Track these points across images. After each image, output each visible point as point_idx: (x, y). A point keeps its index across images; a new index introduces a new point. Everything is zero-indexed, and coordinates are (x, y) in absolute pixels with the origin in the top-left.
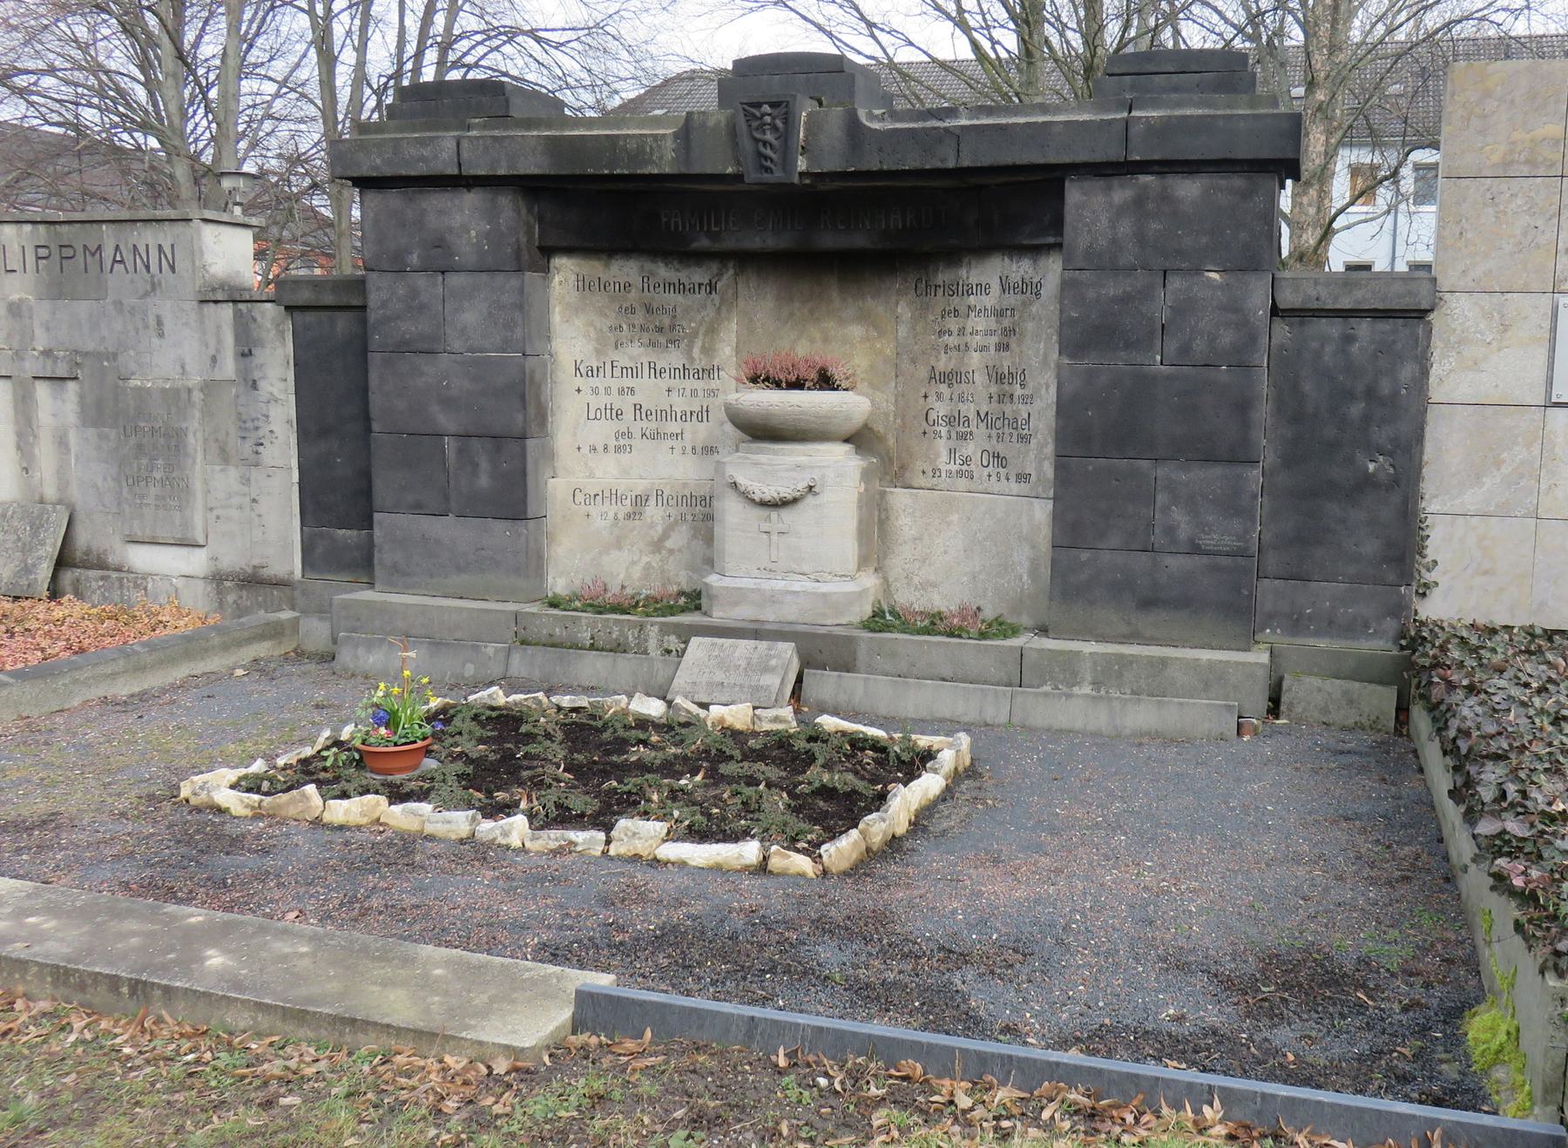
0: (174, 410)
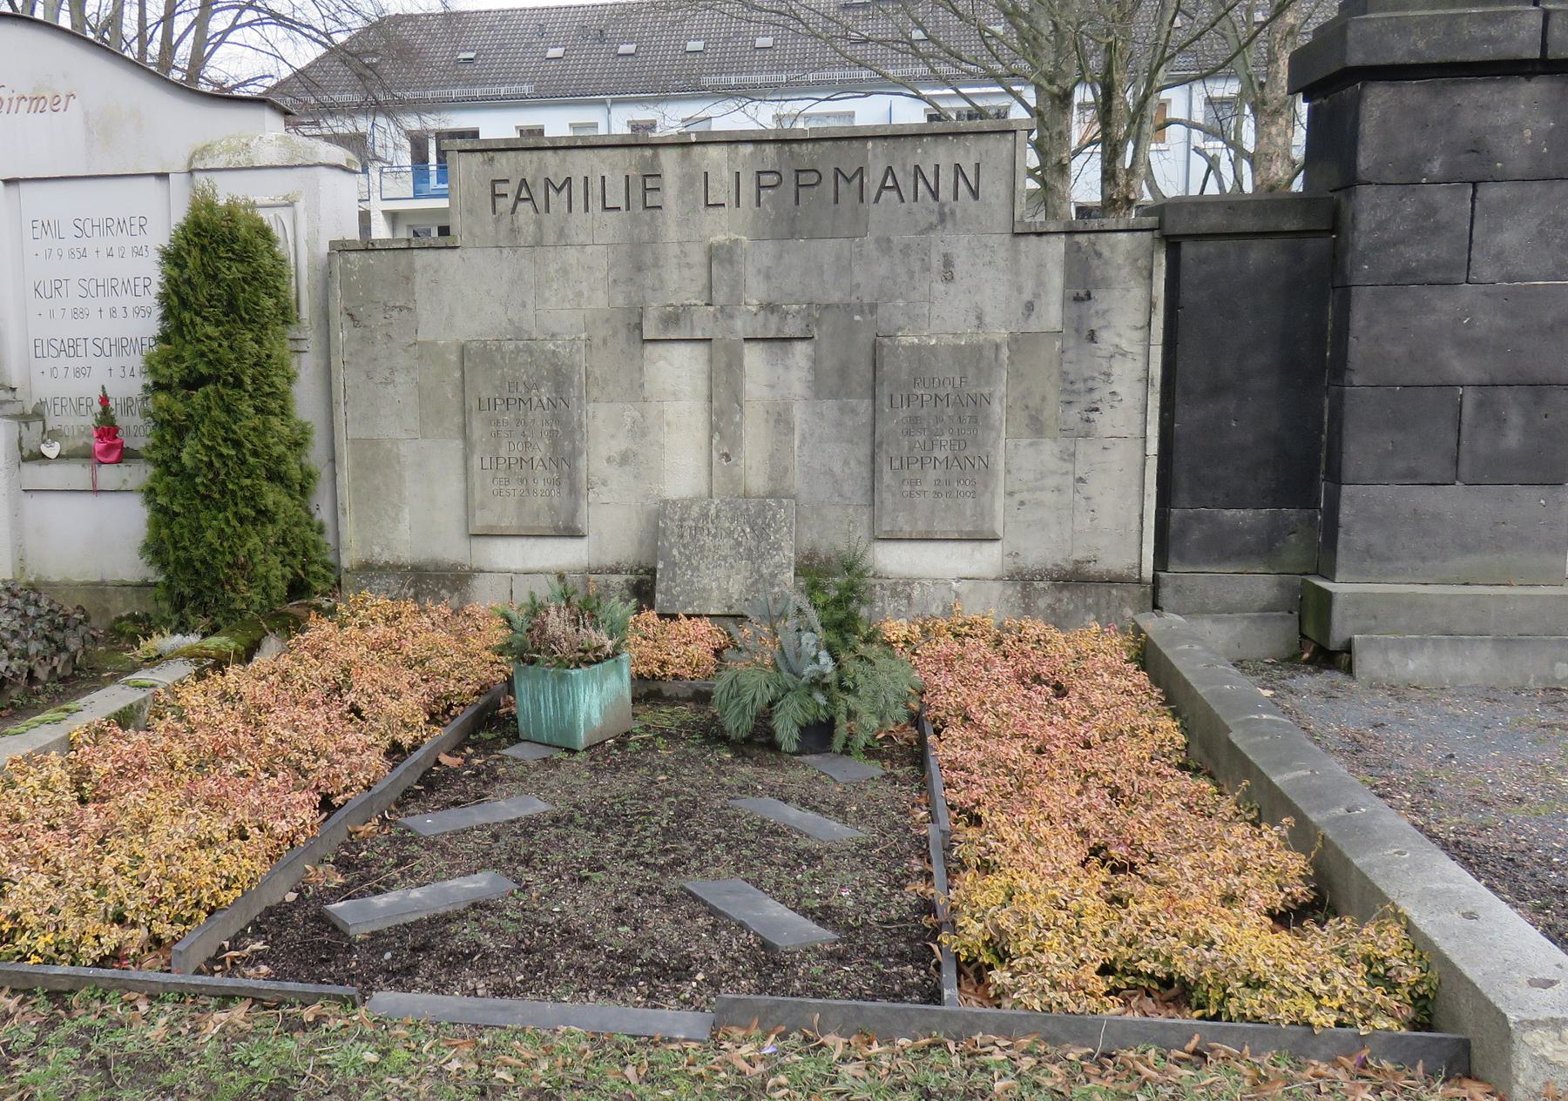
0: (971, 372)
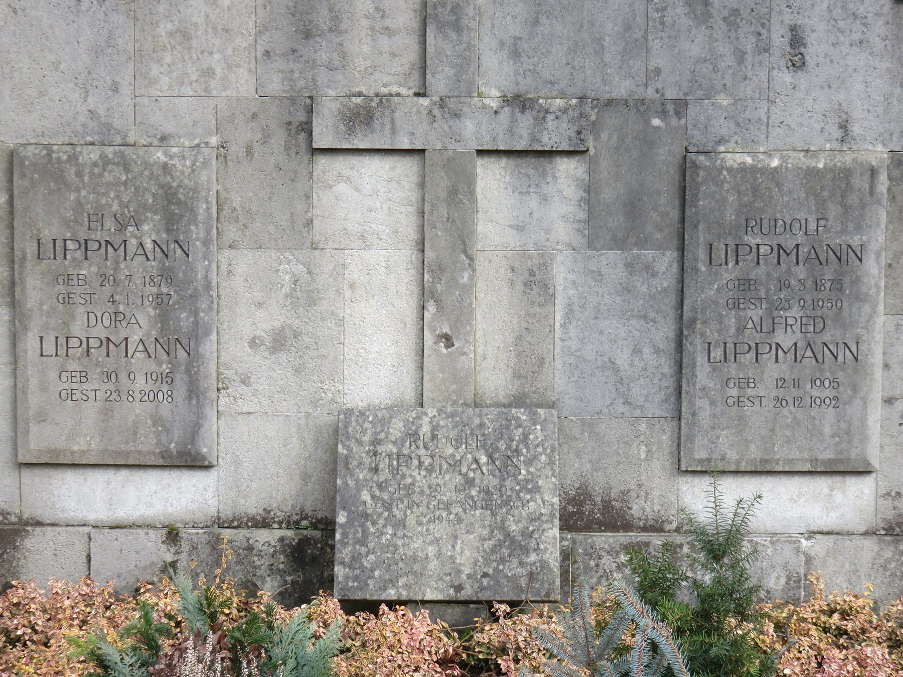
0: (833, 210)
